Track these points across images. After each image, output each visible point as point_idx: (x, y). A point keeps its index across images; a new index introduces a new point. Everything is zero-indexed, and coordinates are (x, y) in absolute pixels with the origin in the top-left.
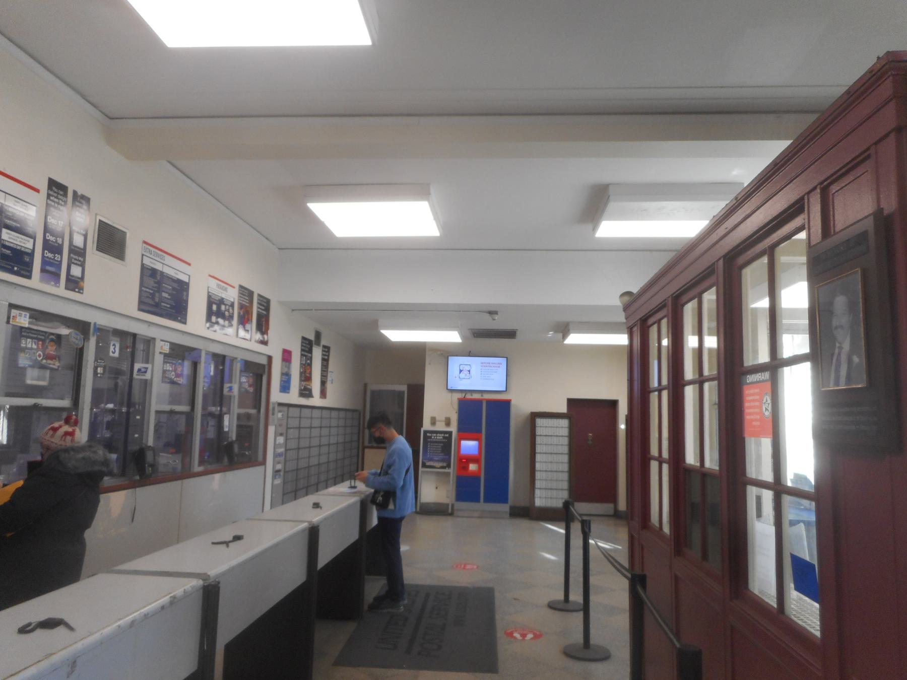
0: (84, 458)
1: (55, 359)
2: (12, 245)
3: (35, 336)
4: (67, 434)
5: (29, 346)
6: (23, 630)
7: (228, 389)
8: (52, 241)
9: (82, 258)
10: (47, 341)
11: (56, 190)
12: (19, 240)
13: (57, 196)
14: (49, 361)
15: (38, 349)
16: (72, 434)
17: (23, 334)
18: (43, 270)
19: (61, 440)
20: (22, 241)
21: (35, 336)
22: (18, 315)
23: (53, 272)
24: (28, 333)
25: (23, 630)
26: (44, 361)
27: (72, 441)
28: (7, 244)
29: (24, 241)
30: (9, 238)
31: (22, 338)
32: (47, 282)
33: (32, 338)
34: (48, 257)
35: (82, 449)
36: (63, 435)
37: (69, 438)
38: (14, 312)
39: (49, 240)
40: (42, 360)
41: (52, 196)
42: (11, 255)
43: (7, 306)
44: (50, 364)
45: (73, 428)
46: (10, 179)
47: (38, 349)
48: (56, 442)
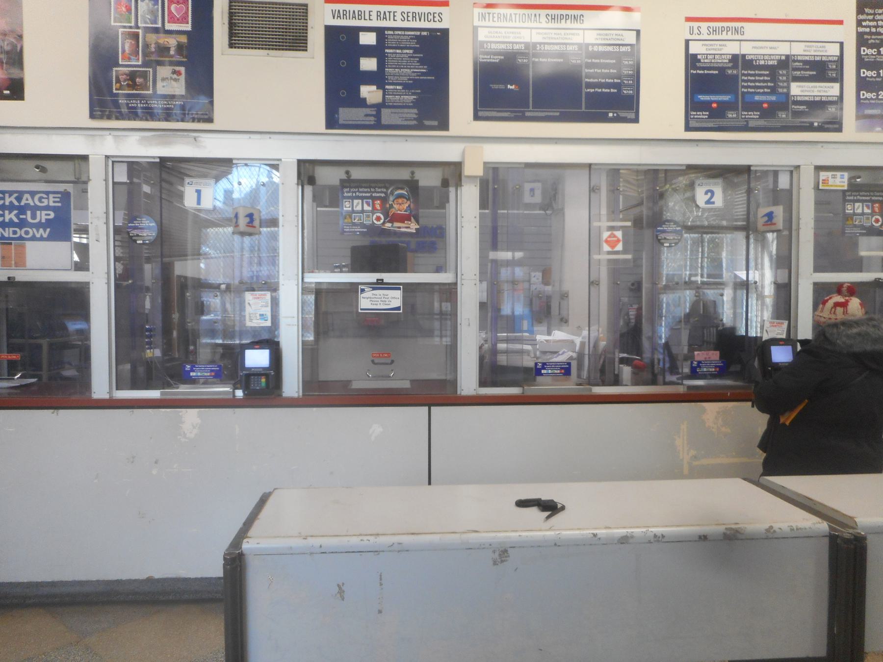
0: (859, 334)
1: (410, 220)
2: (807, 99)
3: (868, 198)
4: (837, 304)
5: (860, 211)
6: (522, 504)
7: (766, 218)
8: (872, 77)
9: (743, 92)
10: (391, 198)
11: (871, 11)
12: (816, 90)
13: (874, 18)
14: (396, 224)
15: (873, 213)
16: (844, 305)
17: (848, 198)
18: (859, 117)
19: (830, 313)
20: (821, 89)
21: (868, 198)
22: (830, 177)
23: (879, 115)
24: (856, 196)
25: (522, 504)
26: (388, 225)
27: (845, 313)
28: (799, 99)
29: (826, 89)
30: (802, 91)
31: (847, 203)
32: (870, 129)
33: (362, 198)
34: (866, 99)
35: (857, 323)
36: (832, 308)
37: (840, 310)
38: (823, 175)
39: (867, 76)
40: (384, 223)
41: (865, 20)
42: (807, 110)
43: (813, 169)
44: (400, 228)
45: (847, 298)
46: (742, 18)
47: (873, 213)
48: (824, 316)
